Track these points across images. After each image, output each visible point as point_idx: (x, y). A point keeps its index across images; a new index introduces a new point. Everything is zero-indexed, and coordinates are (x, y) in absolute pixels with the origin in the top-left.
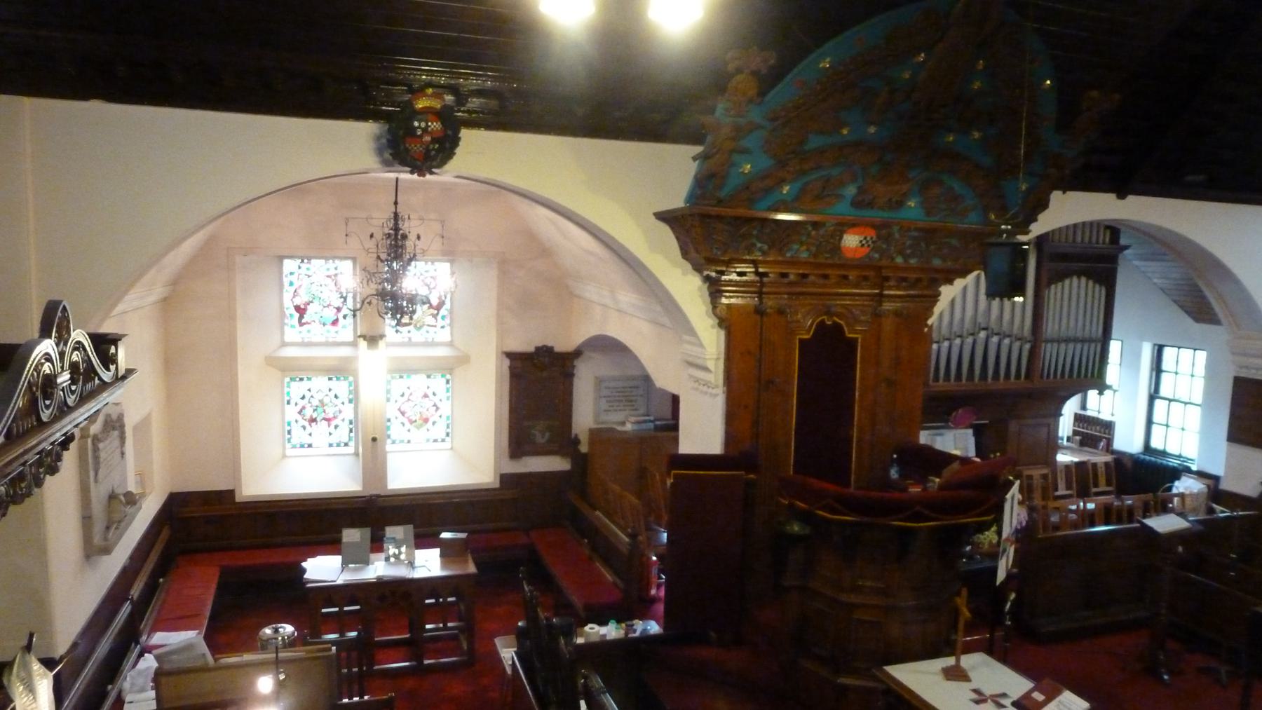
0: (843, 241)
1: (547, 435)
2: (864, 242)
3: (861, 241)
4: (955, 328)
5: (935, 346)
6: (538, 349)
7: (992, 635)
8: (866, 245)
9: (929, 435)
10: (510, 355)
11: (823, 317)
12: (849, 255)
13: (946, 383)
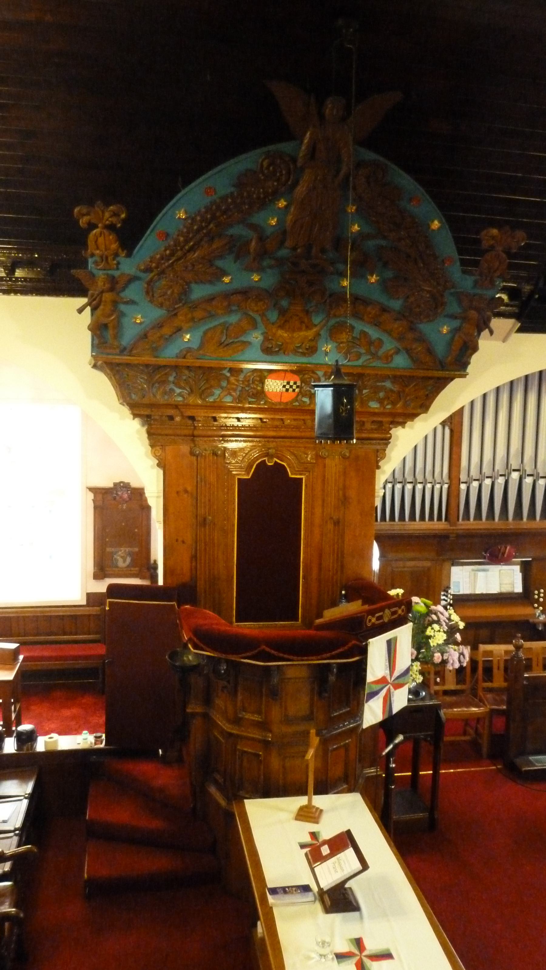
0: (266, 387)
1: (128, 560)
2: (288, 387)
3: (284, 386)
4: (487, 470)
5: (463, 487)
6: (115, 484)
7: (436, 771)
8: (291, 390)
9: (473, 570)
10: (91, 489)
11: (264, 459)
12: (276, 400)
13: (477, 522)
